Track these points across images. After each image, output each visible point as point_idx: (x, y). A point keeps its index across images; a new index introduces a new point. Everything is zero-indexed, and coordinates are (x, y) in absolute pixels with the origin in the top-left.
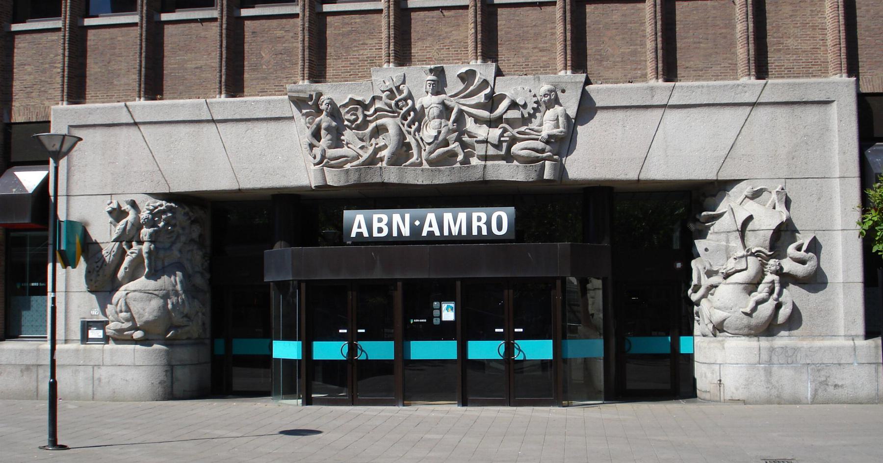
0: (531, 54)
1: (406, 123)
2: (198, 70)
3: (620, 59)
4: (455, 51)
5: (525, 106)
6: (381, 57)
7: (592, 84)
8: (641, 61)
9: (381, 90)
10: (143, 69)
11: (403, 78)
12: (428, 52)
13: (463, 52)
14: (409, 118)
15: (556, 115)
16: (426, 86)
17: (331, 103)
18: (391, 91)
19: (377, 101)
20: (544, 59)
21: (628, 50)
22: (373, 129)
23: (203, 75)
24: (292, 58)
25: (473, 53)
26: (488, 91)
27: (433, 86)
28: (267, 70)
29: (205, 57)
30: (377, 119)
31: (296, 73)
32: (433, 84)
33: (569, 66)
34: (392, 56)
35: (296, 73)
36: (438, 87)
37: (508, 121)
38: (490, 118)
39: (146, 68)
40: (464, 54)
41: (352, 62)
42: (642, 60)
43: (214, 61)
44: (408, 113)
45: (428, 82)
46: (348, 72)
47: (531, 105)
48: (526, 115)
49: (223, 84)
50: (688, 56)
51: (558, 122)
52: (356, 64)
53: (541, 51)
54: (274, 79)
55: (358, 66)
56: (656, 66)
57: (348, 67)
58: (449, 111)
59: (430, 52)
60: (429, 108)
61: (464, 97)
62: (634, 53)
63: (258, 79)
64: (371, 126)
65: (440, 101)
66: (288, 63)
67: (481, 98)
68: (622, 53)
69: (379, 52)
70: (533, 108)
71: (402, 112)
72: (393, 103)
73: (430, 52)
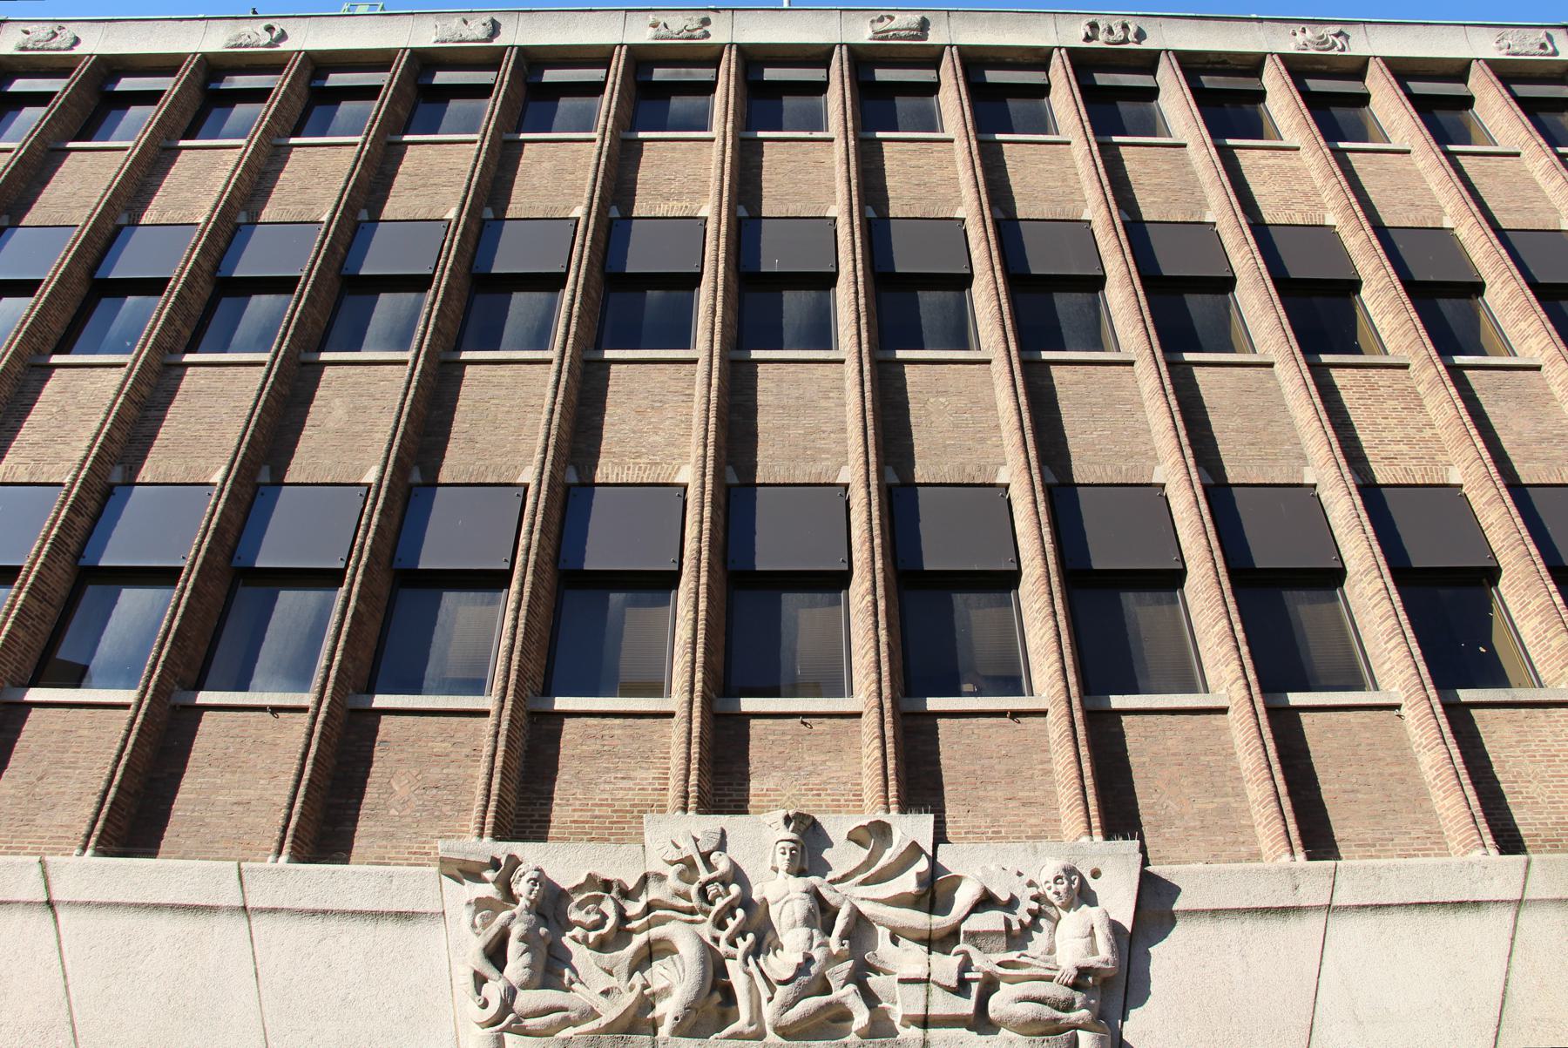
0: (1004, 812)
1: (723, 935)
2: (240, 809)
3: (1198, 823)
4: (833, 801)
5: (1012, 904)
6: (665, 806)
7: (1362, 354)
8: (1242, 826)
9: (666, 862)
10: (113, 790)
11: (718, 836)
12: (771, 801)
13: (851, 803)
14: (732, 924)
15: (1089, 924)
16: (774, 855)
17: (540, 879)
18: (689, 863)
19: (652, 885)
20: (1033, 821)
21: (1211, 806)
22: (640, 949)
23: (249, 820)
24: (460, 798)
25: (880, 796)
26: (923, 865)
27: (791, 853)
28: (397, 819)
29: (262, 782)
30: (649, 926)
31: (465, 829)
32: (791, 850)
33: (1096, 828)
34: (693, 797)
35: (465, 829)
36: (802, 860)
37: (972, 936)
38: (931, 930)
39: (120, 787)
40: (854, 806)
41: (597, 813)
42: (1244, 826)
43: (282, 792)
44: (730, 910)
45: (781, 844)
46: (586, 833)
47: (1026, 905)
48: (1016, 927)
49: (290, 832)
50: (1339, 817)
51: (1093, 942)
52: (607, 817)
53: (1024, 805)
54: (410, 839)
55: (610, 823)
56: (1283, 828)
57: (587, 822)
58: (829, 914)
59: (776, 800)
60: (783, 901)
61: (865, 883)
62: (1225, 811)
63: (373, 835)
64: (638, 940)
65: (808, 886)
66: (449, 807)
67: (907, 883)
68: (1200, 811)
69: (659, 795)
70: (1030, 911)
71: (715, 909)
72: (693, 890)
73: (776, 800)
